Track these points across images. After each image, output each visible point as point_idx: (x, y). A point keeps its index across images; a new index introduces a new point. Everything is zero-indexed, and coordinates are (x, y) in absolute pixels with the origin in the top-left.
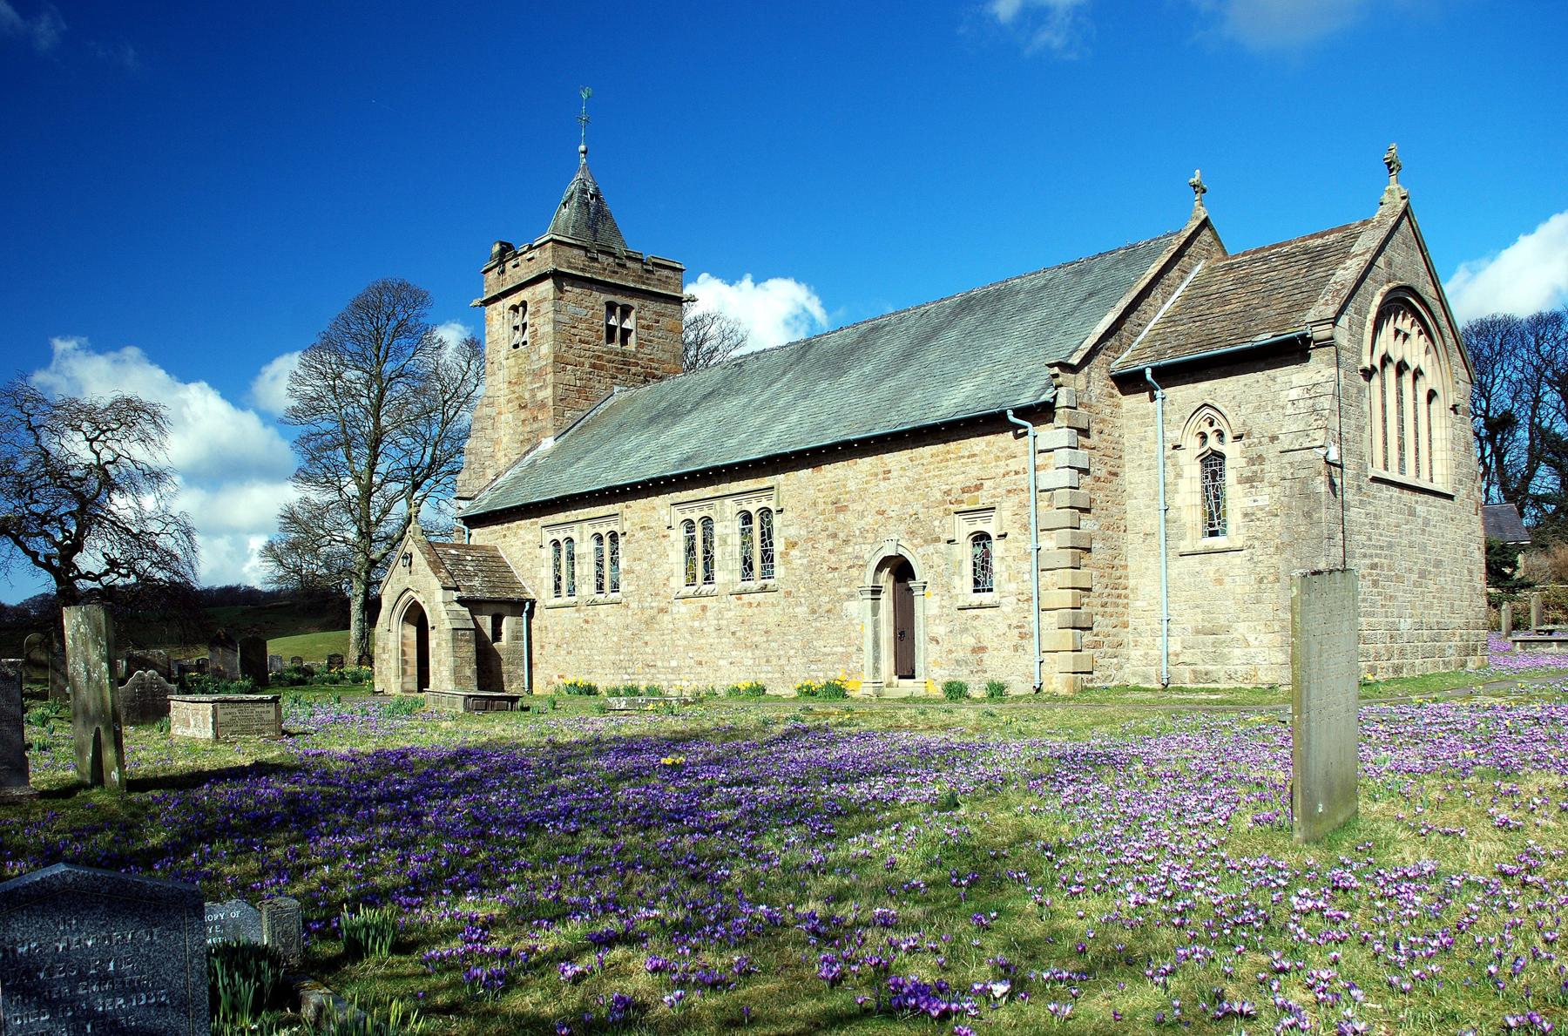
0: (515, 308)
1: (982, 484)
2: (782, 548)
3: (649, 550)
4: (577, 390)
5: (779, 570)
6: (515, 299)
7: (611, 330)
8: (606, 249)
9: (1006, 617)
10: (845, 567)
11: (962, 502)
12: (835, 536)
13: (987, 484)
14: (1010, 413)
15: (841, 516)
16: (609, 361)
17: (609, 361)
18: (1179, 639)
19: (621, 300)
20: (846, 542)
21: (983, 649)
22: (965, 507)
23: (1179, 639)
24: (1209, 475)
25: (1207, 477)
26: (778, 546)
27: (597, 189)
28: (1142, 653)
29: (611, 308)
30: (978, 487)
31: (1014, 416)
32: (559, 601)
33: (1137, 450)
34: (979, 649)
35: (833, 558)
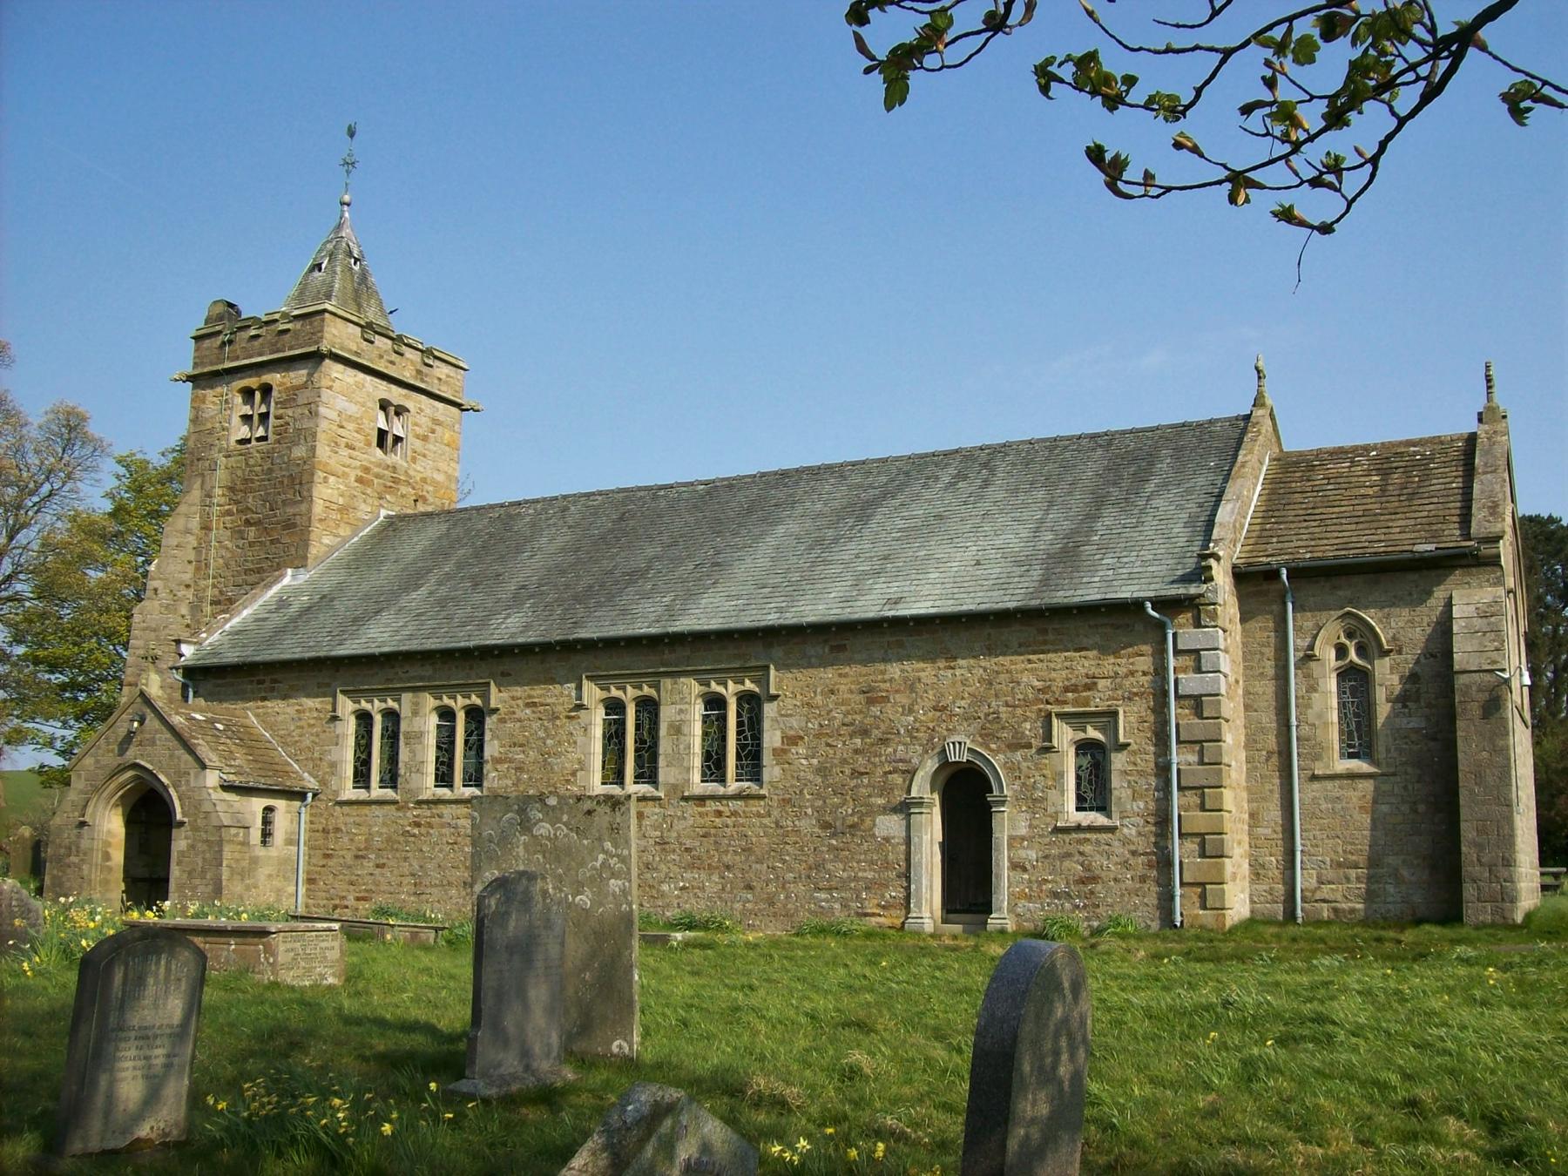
0: (384, 405)
1: (1095, 684)
2: (778, 743)
3: (542, 734)
4: (338, 510)
5: (771, 770)
6: (396, 394)
7: (382, 434)
8: (384, 332)
9: (1126, 842)
10: (879, 771)
11: (1065, 703)
12: (865, 733)
13: (1102, 684)
14: (1149, 605)
15: (875, 710)
16: (378, 476)
17: (378, 476)
18: (1314, 872)
19: (252, 382)
20: (884, 741)
21: (1094, 879)
22: (1068, 709)
23: (1314, 872)
24: (1348, 690)
25: (1345, 693)
26: (771, 738)
27: (361, 252)
28: (1266, 887)
29: (248, 394)
30: (1090, 687)
31: (1153, 609)
32: (362, 794)
33: (1258, 656)
34: (1089, 878)
35: (861, 760)
